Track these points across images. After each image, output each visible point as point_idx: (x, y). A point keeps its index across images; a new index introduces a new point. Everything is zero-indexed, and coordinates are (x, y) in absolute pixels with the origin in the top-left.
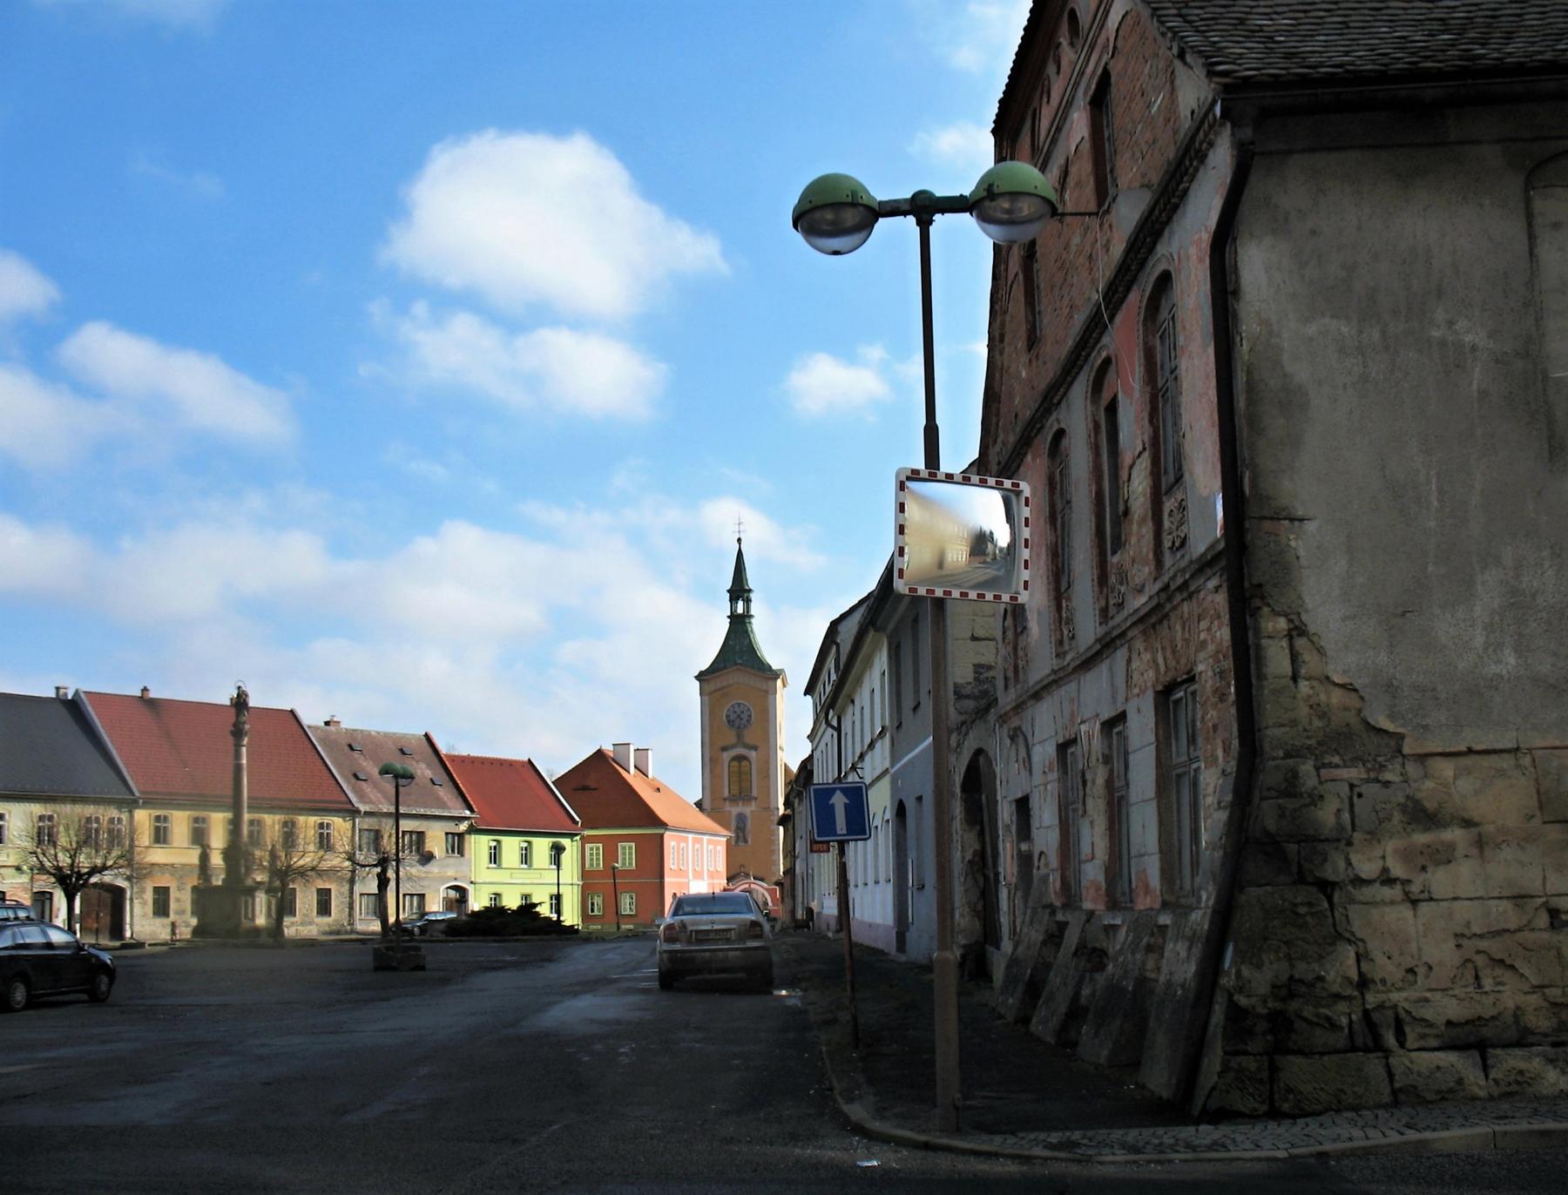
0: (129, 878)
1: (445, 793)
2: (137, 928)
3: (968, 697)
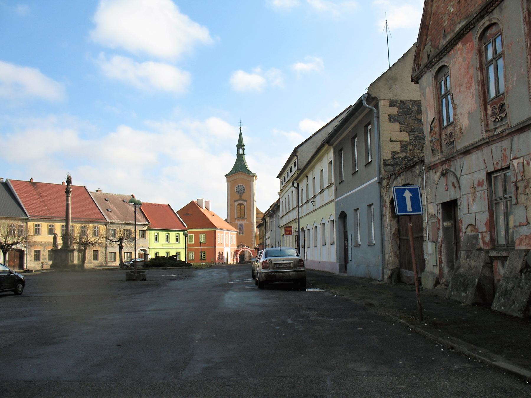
0: (25, 247)
2: (28, 265)
3: (389, 165)
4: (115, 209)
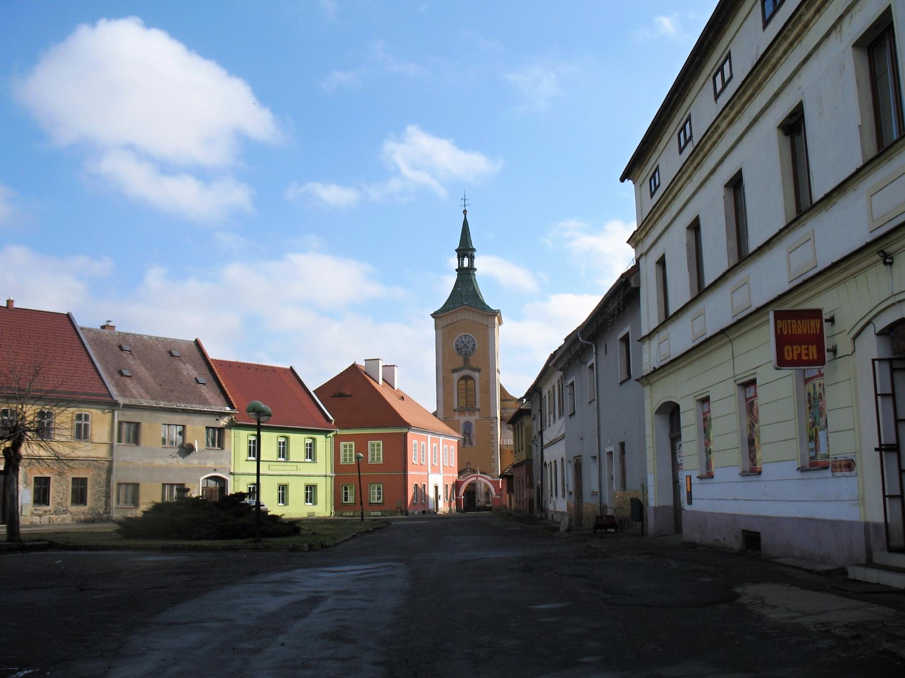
1: (208, 392)
4: (142, 371)
